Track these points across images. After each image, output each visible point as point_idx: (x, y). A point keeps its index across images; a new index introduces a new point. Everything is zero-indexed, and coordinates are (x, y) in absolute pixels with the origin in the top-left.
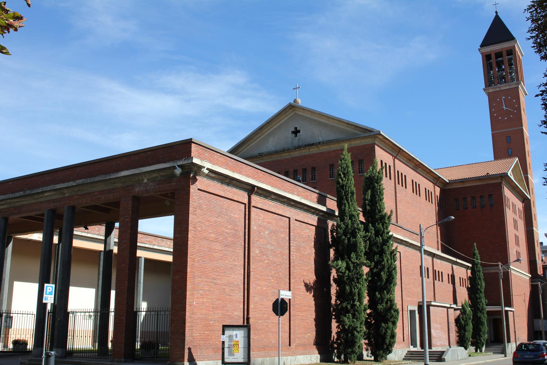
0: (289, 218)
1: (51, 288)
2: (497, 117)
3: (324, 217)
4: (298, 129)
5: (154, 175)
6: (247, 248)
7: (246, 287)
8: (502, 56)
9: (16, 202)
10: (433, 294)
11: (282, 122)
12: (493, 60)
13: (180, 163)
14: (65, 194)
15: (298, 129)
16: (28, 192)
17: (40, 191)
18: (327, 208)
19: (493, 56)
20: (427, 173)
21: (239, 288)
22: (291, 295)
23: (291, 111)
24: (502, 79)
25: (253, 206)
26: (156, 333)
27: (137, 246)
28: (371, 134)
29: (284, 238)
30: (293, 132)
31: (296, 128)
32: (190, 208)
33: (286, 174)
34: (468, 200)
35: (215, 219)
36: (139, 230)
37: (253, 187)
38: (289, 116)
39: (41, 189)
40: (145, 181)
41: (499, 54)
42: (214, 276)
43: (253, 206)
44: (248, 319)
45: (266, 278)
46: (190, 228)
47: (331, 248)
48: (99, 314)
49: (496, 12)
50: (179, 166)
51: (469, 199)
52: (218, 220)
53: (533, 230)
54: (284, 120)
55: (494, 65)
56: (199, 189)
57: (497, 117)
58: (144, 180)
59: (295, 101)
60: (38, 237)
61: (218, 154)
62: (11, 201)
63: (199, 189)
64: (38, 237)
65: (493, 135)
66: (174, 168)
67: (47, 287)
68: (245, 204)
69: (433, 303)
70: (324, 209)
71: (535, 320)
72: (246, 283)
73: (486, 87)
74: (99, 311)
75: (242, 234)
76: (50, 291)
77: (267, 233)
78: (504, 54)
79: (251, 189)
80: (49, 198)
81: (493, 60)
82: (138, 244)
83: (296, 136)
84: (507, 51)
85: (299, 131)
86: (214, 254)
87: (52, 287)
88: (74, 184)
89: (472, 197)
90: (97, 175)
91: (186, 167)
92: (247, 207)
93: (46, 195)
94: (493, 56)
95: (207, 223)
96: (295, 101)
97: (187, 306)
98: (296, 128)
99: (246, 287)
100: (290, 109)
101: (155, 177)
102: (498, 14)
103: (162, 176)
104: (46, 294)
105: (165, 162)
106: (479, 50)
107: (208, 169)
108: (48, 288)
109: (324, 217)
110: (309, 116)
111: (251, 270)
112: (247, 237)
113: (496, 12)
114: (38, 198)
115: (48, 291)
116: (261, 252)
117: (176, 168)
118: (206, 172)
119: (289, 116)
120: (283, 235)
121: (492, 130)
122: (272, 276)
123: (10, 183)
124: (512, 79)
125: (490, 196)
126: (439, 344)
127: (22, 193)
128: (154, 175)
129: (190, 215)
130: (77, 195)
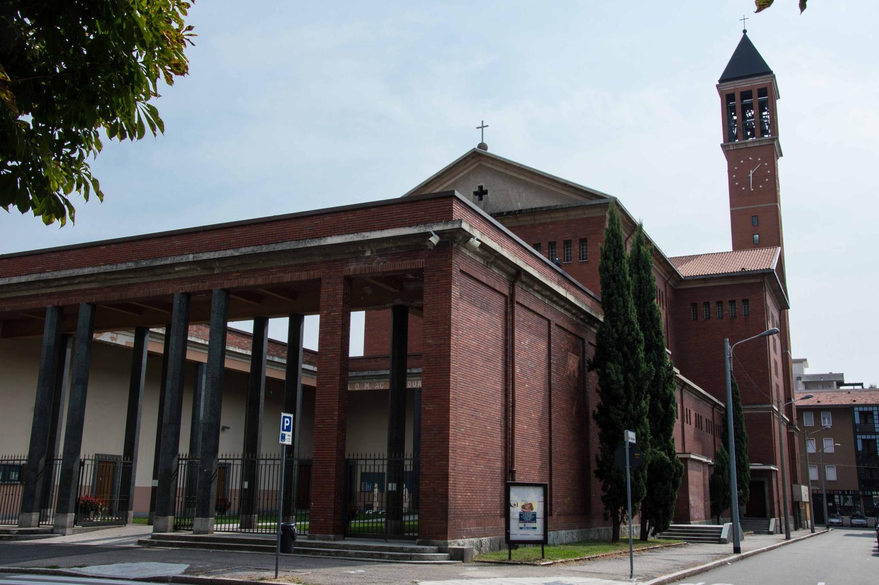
0: (549, 321)
2: (739, 187)
5: (386, 245)
9: (118, 279)
11: (458, 177)
12: (737, 103)
14: (213, 269)
16: (144, 264)
17: (168, 262)
19: (738, 97)
20: (660, 263)
23: (474, 161)
26: (266, 493)
27: (209, 350)
28: (602, 201)
30: (476, 193)
31: (481, 187)
37: (519, 270)
38: (471, 168)
39: (170, 259)
40: (368, 254)
41: (746, 95)
43: (518, 303)
44: (513, 473)
48: (386, 462)
50: (436, 232)
51: (713, 305)
54: (462, 174)
55: (739, 109)
58: (365, 252)
60: (125, 339)
62: (108, 277)
63: (461, 271)
64: (125, 339)
65: (731, 212)
66: (429, 235)
67: (285, 417)
71: (794, 486)
73: (724, 141)
74: (386, 457)
78: (755, 94)
79: (517, 275)
80: (183, 275)
83: (481, 199)
84: (759, 90)
85: (486, 192)
87: (290, 418)
88: (237, 254)
89: (717, 302)
90: (283, 241)
91: (447, 235)
93: (177, 269)
94: (738, 97)
96: (482, 146)
98: (481, 187)
100: (473, 158)
101: (387, 248)
103: (400, 247)
104: (283, 430)
106: (717, 86)
107: (478, 240)
110: (503, 170)
113: (745, 31)
114: (162, 274)
115: (286, 424)
119: (471, 168)
121: (731, 206)
126: (696, 517)
127: (131, 265)
128: (386, 245)
130: (238, 272)
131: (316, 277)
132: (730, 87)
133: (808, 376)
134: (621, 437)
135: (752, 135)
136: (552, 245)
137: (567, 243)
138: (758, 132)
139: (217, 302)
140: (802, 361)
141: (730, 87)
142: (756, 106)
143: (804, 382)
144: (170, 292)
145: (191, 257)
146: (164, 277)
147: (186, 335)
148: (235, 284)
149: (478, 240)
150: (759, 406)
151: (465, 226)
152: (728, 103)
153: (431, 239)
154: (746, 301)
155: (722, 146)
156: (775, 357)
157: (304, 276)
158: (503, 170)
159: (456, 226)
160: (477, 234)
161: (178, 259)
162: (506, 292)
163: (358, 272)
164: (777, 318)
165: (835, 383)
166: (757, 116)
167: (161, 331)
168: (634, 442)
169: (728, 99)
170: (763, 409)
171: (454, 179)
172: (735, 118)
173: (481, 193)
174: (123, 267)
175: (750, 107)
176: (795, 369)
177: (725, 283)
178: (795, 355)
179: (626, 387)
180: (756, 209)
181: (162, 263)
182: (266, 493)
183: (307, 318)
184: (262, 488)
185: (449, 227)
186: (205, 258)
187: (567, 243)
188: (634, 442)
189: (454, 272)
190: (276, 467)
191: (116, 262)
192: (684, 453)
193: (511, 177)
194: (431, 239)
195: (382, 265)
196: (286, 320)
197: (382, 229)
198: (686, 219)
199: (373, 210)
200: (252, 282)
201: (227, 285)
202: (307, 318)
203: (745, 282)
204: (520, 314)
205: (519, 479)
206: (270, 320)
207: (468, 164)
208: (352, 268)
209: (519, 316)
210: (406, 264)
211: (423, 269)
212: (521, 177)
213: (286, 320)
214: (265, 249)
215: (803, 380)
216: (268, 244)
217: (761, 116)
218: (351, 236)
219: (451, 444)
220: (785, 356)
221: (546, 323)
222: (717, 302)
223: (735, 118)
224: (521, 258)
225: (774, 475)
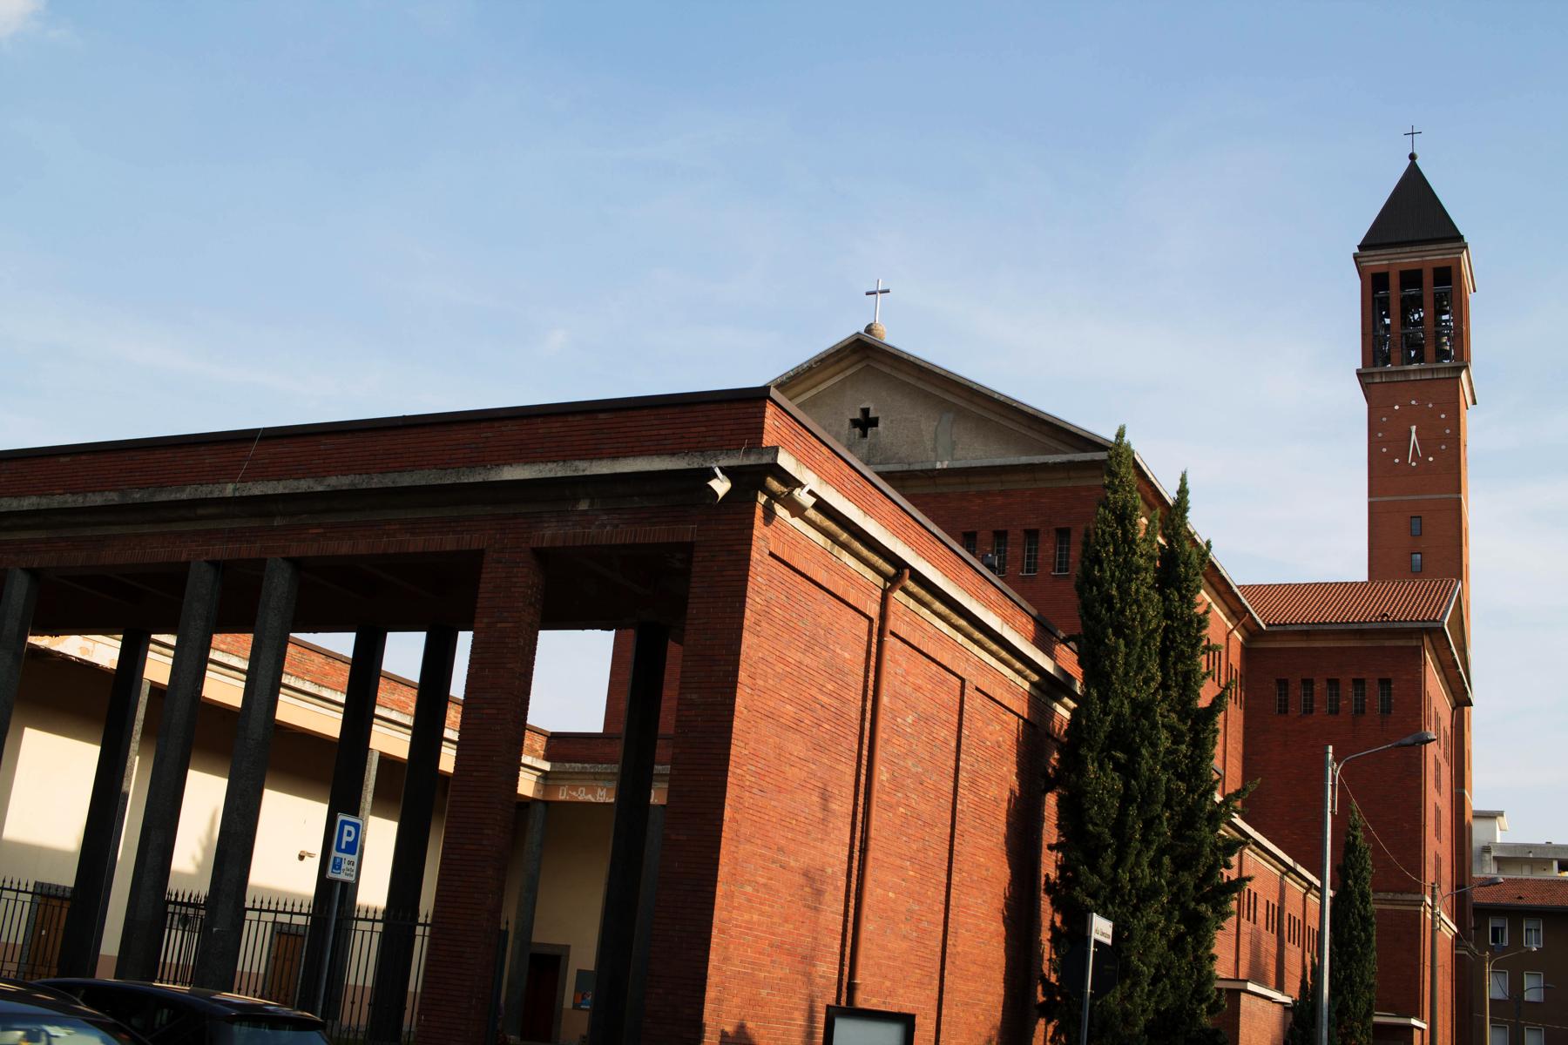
0: (963, 680)
1: (352, 829)
2: (1390, 456)
3: (1049, 687)
4: (872, 415)
6: (864, 762)
7: (854, 886)
8: (1386, 287)
10: (1233, 958)
12: (1395, 293)
13: (725, 462)
15: (872, 415)
16: (138, 496)
17: (184, 496)
18: (1058, 668)
19: (1394, 281)
21: (836, 888)
22: (1110, 931)
24: (1413, 346)
25: (893, 634)
26: (359, 993)
29: (946, 742)
30: (855, 423)
31: (865, 411)
32: (748, 613)
33: (969, 540)
34: (1317, 687)
35: (799, 656)
36: (384, 668)
41: (1411, 278)
42: (783, 842)
43: (893, 634)
44: (852, 988)
45: (899, 862)
46: (743, 676)
47: (1051, 790)
49: (1412, 157)
51: (1320, 687)
52: (807, 661)
53: (1463, 795)
55: (1395, 306)
56: (771, 554)
57: (1390, 456)
59: (869, 329)
60: (103, 651)
61: (824, 449)
63: (771, 554)
64: (103, 651)
65: (1370, 504)
67: (344, 823)
68: (871, 620)
69: (1251, 987)
70: (1047, 665)
72: (855, 872)
75: (855, 714)
76: (351, 839)
77: (910, 720)
78: (1428, 278)
79: (898, 572)
81: (1395, 293)
82: (378, 711)
83: (865, 435)
86: (787, 768)
88: (320, 489)
89: (1329, 681)
92: (875, 630)
94: (1394, 281)
95: (779, 668)
97: (715, 932)
98: (865, 411)
99: (854, 886)
100: (854, 351)
102: (1417, 161)
104: (339, 849)
105: (673, 453)
106: (1356, 257)
107: (811, 492)
108: (347, 828)
109: (1049, 687)
111: (873, 833)
112: (867, 725)
113: (1412, 157)
115: (346, 839)
116: (894, 778)
117: (715, 476)
118: (808, 501)
120: (944, 733)
121: (1372, 492)
122: (910, 859)
123: (62, 460)
124: (1442, 354)
125: (1385, 683)
127: (113, 498)
129: (745, 634)
130: (319, 526)
131: (474, 547)
132: (1379, 261)
133: (1504, 847)
134: (1085, 925)
135: (1420, 358)
136: (1000, 536)
137: (1032, 535)
138: (1430, 351)
139: (279, 587)
140: (1491, 816)
141: (1379, 261)
142: (1428, 300)
143: (1495, 858)
144: (184, 558)
145: (229, 490)
146: (175, 527)
147: (279, 672)
148: (311, 550)
149: (811, 492)
150: (1399, 896)
151: (785, 461)
152: (1375, 291)
153: (714, 484)
154: (1385, 683)
155: (1360, 374)
156: (1436, 799)
157: (450, 543)
158: (912, 381)
159: (766, 460)
160: (810, 479)
161: (205, 491)
162: (873, 610)
163: (559, 544)
164: (1446, 722)
165: (1555, 864)
166: (1429, 323)
167: (171, 639)
168: (1109, 941)
169: (1375, 287)
170: (1404, 902)
171: (814, 392)
172: (1388, 321)
173: (865, 423)
174: (96, 500)
175: (1416, 302)
176: (1479, 833)
177: (1346, 644)
178: (1477, 800)
179: (1119, 828)
180: (1417, 505)
181: (173, 497)
182: (359, 993)
183: (461, 634)
184: (352, 982)
185: (752, 460)
186: (257, 492)
187: (1032, 535)
188: (1109, 941)
189: (755, 555)
190: (262, 925)
191: (84, 491)
192: (1237, 980)
193: (927, 395)
194: (714, 484)
195: (605, 528)
196: (419, 638)
197: (615, 456)
198: (1281, 515)
199: (602, 416)
200: (344, 548)
201: (295, 551)
202: (461, 634)
203: (1387, 643)
204: (896, 656)
205: (863, 1001)
206: (389, 635)
207: (843, 364)
208: (548, 533)
209: (896, 662)
210: (657, 533)
211: (692, 544)
212: (948, 397)
213: (419, 638)
214: (377, 481)
215: (1494, 854)
216: (383, 472)
217: (1438, 323)
218: (550, 465)
219: (718, 915)
220: (1459, 801)
221: (958, 682)
222: (1329, 681)
223: (1388, 321)
224: (908, 542)
225: (1417, 1033)
